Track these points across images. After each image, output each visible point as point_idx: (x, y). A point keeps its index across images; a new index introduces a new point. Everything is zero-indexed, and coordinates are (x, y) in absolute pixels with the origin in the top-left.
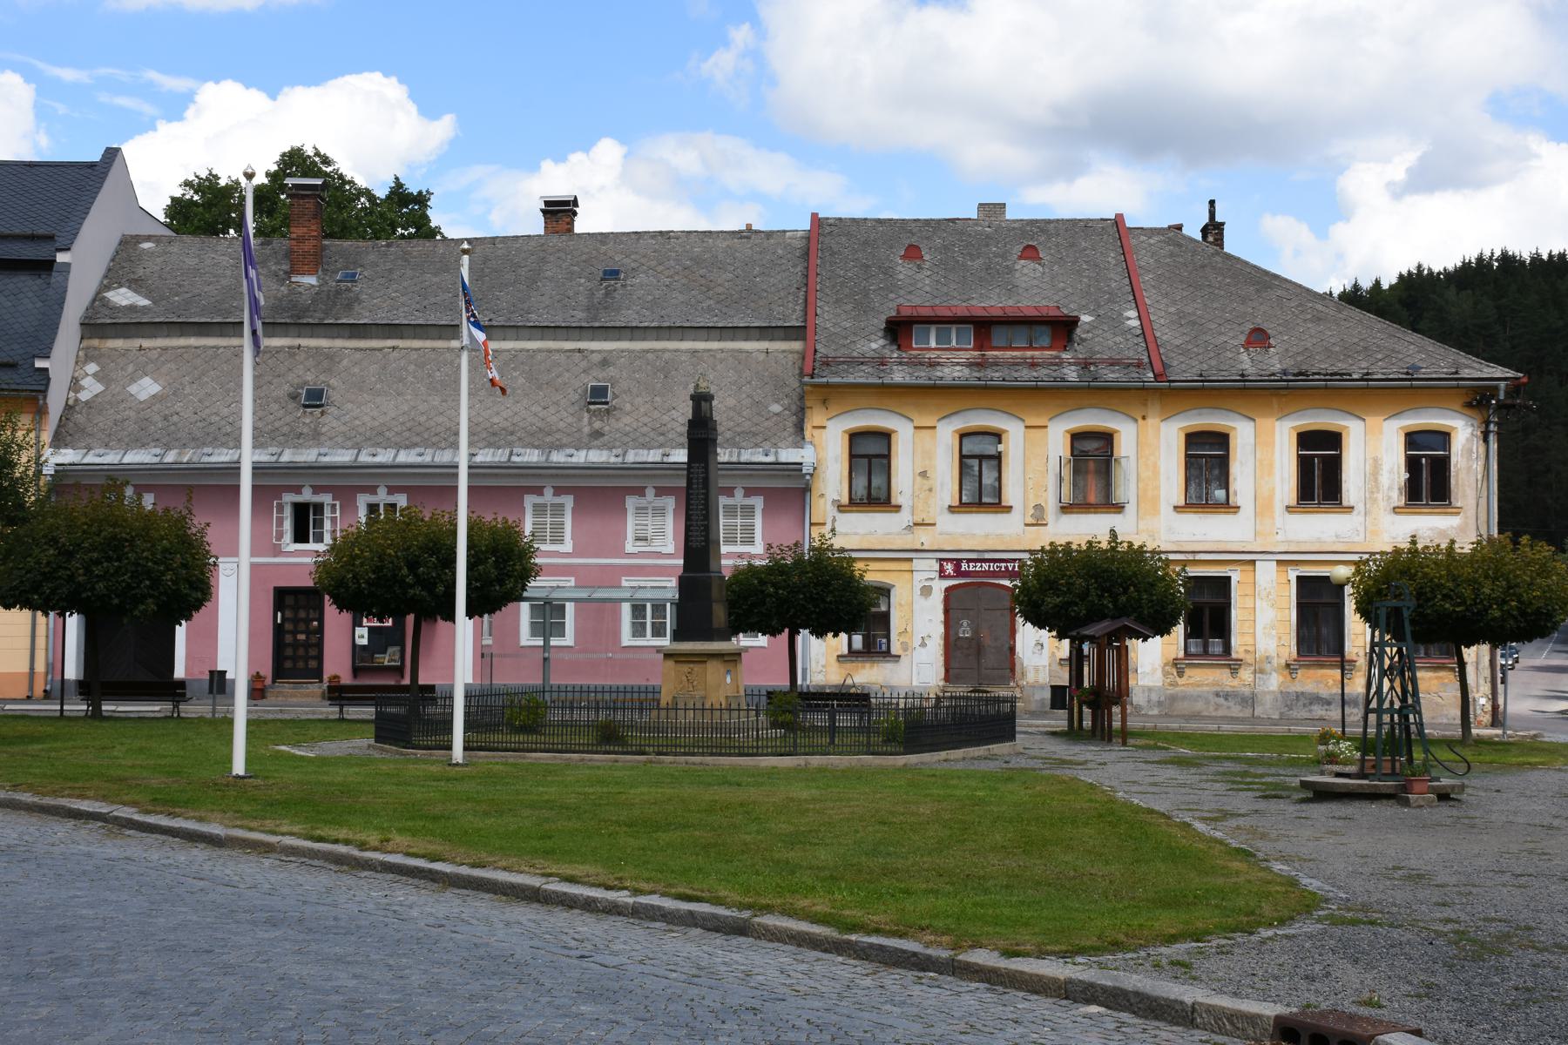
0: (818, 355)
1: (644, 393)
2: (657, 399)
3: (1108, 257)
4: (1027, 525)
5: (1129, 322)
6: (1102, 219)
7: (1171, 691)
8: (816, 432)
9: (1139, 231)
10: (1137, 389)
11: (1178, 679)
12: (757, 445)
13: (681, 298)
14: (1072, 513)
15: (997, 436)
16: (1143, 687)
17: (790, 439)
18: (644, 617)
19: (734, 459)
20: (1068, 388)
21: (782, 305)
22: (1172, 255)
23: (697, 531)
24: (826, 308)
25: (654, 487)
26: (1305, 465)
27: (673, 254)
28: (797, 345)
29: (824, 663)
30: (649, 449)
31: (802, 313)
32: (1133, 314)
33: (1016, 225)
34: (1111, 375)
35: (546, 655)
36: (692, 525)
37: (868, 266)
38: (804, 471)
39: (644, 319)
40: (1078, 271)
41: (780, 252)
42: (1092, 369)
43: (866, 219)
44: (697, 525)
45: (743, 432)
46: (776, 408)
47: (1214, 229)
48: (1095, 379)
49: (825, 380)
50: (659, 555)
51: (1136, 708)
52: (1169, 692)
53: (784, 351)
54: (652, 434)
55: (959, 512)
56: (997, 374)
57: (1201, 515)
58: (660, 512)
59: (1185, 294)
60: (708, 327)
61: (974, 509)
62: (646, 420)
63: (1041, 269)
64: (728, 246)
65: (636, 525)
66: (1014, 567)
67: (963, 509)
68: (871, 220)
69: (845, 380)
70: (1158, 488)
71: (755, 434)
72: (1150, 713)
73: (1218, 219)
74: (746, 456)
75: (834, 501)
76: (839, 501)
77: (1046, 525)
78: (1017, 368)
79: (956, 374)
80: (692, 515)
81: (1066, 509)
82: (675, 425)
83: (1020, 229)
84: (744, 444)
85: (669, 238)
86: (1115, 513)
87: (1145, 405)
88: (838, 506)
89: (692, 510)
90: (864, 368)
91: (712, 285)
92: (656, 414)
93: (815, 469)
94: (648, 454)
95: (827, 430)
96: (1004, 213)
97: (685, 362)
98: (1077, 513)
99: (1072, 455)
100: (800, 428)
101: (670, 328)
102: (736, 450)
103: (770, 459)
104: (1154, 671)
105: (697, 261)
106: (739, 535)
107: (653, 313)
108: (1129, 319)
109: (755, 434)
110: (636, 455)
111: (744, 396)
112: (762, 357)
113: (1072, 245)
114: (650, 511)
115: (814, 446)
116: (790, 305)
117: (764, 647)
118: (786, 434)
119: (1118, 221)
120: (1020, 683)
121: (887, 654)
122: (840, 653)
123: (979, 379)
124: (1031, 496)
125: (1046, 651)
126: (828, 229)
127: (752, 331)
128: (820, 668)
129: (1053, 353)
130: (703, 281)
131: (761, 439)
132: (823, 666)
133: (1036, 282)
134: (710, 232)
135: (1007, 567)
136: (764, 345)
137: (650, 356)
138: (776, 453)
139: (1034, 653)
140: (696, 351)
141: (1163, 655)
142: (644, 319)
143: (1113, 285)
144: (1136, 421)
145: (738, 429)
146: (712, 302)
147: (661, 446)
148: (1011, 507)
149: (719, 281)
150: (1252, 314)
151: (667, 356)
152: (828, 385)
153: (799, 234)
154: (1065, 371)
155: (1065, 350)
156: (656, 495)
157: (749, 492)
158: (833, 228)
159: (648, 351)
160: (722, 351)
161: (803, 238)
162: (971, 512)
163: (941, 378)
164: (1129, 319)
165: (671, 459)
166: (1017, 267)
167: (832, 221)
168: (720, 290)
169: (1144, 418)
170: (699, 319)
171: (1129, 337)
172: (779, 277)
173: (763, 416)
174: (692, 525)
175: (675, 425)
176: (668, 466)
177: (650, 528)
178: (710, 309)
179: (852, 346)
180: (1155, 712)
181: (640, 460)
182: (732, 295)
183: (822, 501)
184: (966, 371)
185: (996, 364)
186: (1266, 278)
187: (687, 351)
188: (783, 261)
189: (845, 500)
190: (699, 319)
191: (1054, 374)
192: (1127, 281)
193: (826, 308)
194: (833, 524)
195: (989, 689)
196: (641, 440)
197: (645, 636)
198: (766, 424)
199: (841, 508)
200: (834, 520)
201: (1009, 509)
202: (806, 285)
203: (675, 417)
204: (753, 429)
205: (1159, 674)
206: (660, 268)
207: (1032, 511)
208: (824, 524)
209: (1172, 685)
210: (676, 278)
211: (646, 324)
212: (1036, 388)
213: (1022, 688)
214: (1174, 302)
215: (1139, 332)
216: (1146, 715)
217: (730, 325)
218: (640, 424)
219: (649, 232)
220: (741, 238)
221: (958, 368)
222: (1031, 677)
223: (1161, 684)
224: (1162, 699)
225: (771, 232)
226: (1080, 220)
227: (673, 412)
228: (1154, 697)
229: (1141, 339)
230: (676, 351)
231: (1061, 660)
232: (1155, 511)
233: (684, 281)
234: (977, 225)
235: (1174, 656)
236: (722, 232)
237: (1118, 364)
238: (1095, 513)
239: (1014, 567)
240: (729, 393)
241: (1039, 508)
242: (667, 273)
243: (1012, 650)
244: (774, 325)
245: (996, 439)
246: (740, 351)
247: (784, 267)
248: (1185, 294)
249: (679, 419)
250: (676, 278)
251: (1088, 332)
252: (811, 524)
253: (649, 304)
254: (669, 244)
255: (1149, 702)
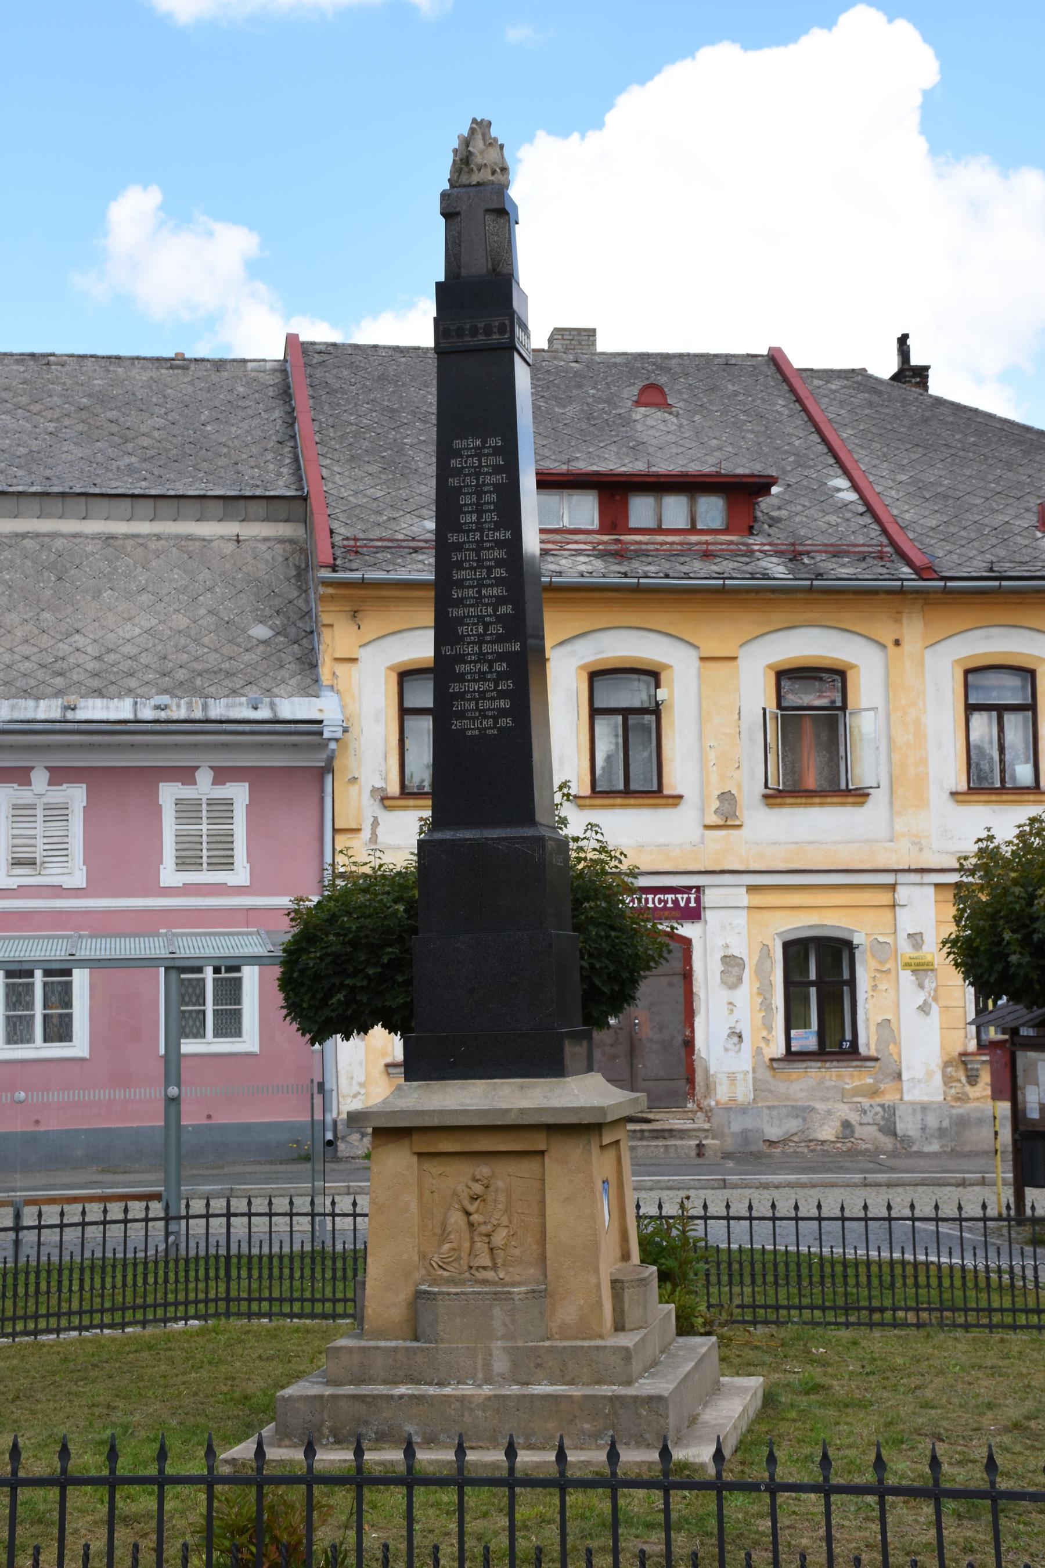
0: (337, 539)
1: (20, 606)
2: (46, 615)
3: (775, 404)
4: (708, 827)
5: (840, 495)
6: (748, 355)
7: (960, 1109)
8: (341, 669)
9: (809, 373)
10: (890, 592)
11: (968, 1088)
12: (234, 692)
13: (79, 452)
14: (781, 805)
15: (653, 675)
16: (912, 1103)
17: (293, 682)
18: (30, 1005)
19: (198, 714)
20: (774, 590)
21: (257, 466)
22: (871, 404)
23: (482, 677)
24: (336, 469)
25: (47, 768)
26: (10, 990)
27: (58, 388)
28: (285, 530)
29: (362, 1079)
30: (38, 698)
31: (293, 479)
32: (842, 483)
33: (618, 360)
34: (843, 570)
35: (173, 1091)
36: (461, 659)
37: (393, 411)
38: (326, 735)
39: (15, 481)
40: (734, 423)
41: (241, 389)
42: (806, 560)
43: (376, 347)
44: (482, 657)
45: (207, 671)
46: (261, 632)
47: (913, 376)
48: (819, 576)
49: (357, 575)
50: (58, 891)
51: (902, 1141)
52: (954, 1111)
53: (266, 539)
54: (40, 674)
55: (592, 806)
56: (652, 569)
57: (996, 807)
58: (59, 813)
59: (914, 456)
60: (133, 496)
61: (619, 801)
62: (27, 650)
63: (674, 420)
64: (152, 378)
65: (14, 837)
66: (688, 900)
67: (599, 801)
68: (385, 347)
69: (392, 576)
70: (923, 761)
71: (229, 675)
72: (927, 1149)
73: (915, 360)
74: (217, 710)
75: (374, 790)
76: (382, 789)
77: (739, 826)
78: (682, 559)
79: (583, 568)
80: (460, 621)
81: (774, 797)
82: (81, 658)
83: (626, 365)
84: (212, 689)
85: (48, 364)
86: (854, 804)
87: (898, 621)
88: (383, 799)
89: (459, 603)
90: (421, 557)
91: (131, 434)
92: (45, 641)
93: (346, 730)
94: (37, 707)
95: (360, 665)
96: (594, 343)
97: (93, 554)
98: (791, 805)
99: (779, 706)
100: (309, 664)
101: (63, 495)
102: (200, 701)
103: (264, 714)
104: (930, 1074)
105: (101, 398)
106: (205, 853)
107: (30, 472)
108: (839, 490)
109: (229, 675)
110: (13, 708)
111: (203, 611)
112: (230, 547)
113: (713, 389)
114: (40, 812)
115: (338, 692)
116: (272, 466)
117: (82, 1060)
118: (284, 673)
119: (775, 360)
120: (704, 1104)
121: (852, 1053)
122: (389, 1060)
123: (626, 575)
124: (714, 778)
125: (747, 1045)
126: (317, 359)
127: (211, 503)
128: (355, 1088)
129: (734, 538)
130: (115, 429)
131: (242, 683)
132: (361, 1085)
133: (671, 438)
134: (118, 358)
135: (676, 902)
136: (231, 528)
137: (28, 543)
138: (272, 706)
139: (726, 1050)
140: (111, 537)
141: (942, 1048)
142: (15, 481)
143: (797, 443)
144: (884, 647)
145: (198, 666)
146: (133, 459)
147: (59, 693)
148: (681, 797)
149: (143, 429)
150: (1031, 484)
151: (59, 544)
152: (363, 584)
153: (269, 366)
154: (763, 564)
155: (752, 534)
156: (51, 783)
157: (222, 775)
158: (326, 357)
159: (24, 536)
160: (159, 537)
161: (275, 370)
162: (612, 806)
163: (560, 574)
164: (839, 490)
165: (81, 715)
166: (637, 416)
167: (323, 348)
168: (146, 442)
169: (897, 643)
170: (114, 484)
171: (848, 515)
172: (245, 425)
173: (239, 646)
174: (461, 659)
175: (81, 658)
176: (76, 726)
177: (40, 841)
178: (131, 470)
179: (393, 525)
180: (935, 1147)
181: (21, 715)
182: (167, 451)
183: (353, 790)
184: (598, 565)
185: (646, 554)
186: (1029, 436)
187: (95, 537)
188: (248, 403)
189: (394, 789)
190: (114, 484)
191: (748, 568)
192: (816, 438)
193: (336, 469)
194: (374, 833)
195: (651, 1116)
196: (20, 683)
197: (204, 1036)
198: (247, 657)
199: (385, 800)
200: (375, 823)
201: (677, 799)
202: (293, 437)
203: (80, 645)
204: (225, 666)
205: (938, 1079)
206: (36, 408)
207: (716, 804)
208: (357, 830)
209: (959, 1099)
210: (67, 422)
211: (20, 489)
212: (723, 591)
213: (708, 1113)
214: (902, 468)
215: (862, 509)
216: (920, 1154)
217: (172, 493)
218: (17, 657)
219: (11, 355)
220: (172, 367)
221: (582, 559)
222: (722, 1093)
223: (941, 1098)
224: (946, 1123)
225: (221, 360)
226: (716, 356)
227: (77, 637)
228: (932, 1121)
229: (867, 520)
230: (76, 536)
231: (772, 1060)
232: (921, 802)
233: (80, 427)
234: (555, 358)
235: (959, 1049)
236: (138, 358)
237: (847, 553)
238: (822, 804)
239: (688, 900)
240: (176, 606)
241: (726, 797)
242: (49, 414)
243: (689, 1044)
244: (248, 493)
245: (652, 680)
246: (190, 538)
247: (250, 412)
248: (914, 456)
249: (89, 650)
250: (67, 422)
251: (779, 508)
252: (335, 831)
253: (22, 461)
254: (48, 372)
255: (923, 1129)
